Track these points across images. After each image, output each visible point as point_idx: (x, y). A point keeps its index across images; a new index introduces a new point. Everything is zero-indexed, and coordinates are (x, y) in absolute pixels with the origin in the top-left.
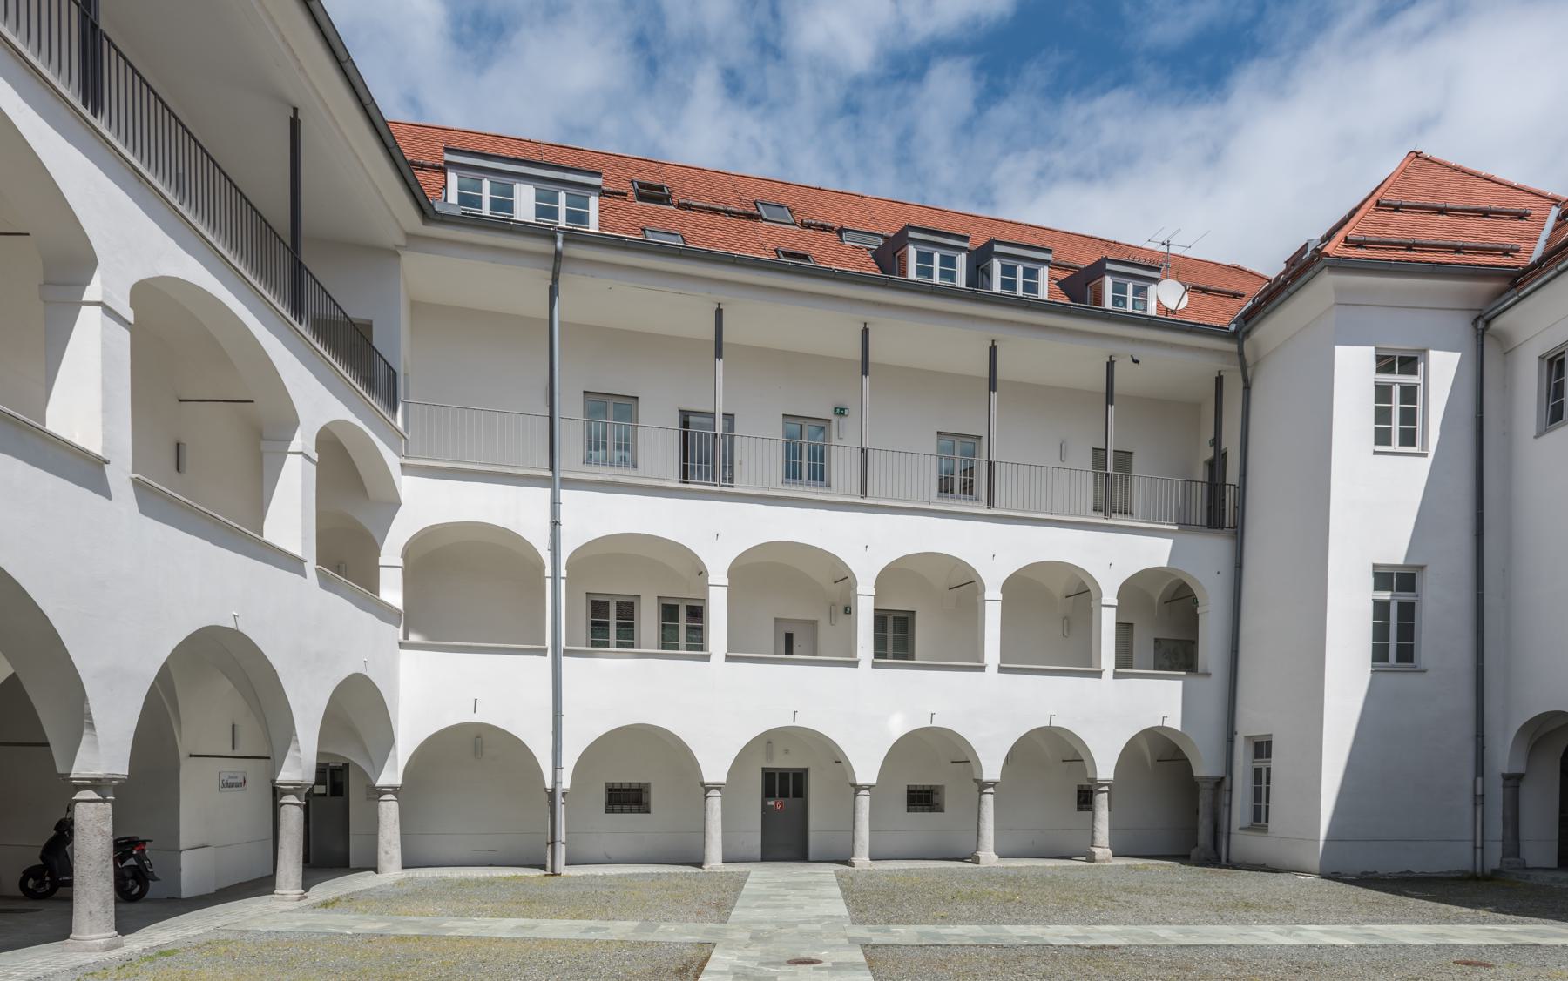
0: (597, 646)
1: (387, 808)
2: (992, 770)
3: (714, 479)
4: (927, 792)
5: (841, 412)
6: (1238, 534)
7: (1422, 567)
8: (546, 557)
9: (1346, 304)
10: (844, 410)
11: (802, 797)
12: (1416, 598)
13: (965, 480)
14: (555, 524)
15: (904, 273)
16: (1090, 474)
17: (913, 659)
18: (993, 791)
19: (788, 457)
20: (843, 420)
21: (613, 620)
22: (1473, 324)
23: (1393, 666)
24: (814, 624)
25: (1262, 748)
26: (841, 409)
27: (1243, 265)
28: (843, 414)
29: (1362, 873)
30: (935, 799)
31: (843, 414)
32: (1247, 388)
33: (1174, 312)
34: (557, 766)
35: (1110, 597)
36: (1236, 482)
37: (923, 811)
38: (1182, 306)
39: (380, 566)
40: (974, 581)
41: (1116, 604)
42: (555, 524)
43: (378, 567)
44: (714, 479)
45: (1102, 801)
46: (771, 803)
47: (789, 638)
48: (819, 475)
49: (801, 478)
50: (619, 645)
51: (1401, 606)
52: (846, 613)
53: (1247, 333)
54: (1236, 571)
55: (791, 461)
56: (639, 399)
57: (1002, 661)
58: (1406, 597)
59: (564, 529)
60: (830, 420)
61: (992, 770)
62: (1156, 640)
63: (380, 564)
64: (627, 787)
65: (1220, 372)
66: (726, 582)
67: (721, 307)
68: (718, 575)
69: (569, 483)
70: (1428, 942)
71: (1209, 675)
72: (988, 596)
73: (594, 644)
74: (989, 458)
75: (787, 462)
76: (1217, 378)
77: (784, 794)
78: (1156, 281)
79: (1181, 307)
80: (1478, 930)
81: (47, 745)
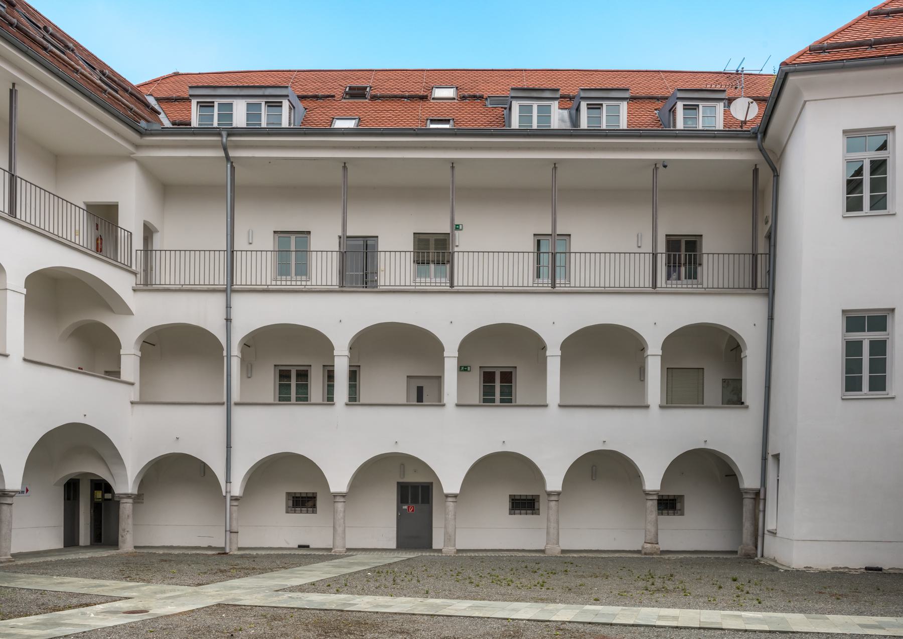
0: (283, 401)
1: (123, 508)
6: (770, 294)
7: (893, 310)
8: (222, 339)
9: (815, 100)
10: (467, 367)
11: (429, 503)
12: (887, 337)
14: (228, 320)
15: (675, 126)
16: (664, 255)
21: (293, 383)
23: (866, 394)
29: (833, 568)
33: (745, 122)
34: (228, 481)
42: (228, 320)
46: (405, 507)
47: (420, 390)
50: (502, 401)
51: (873, 343)
56: (571, 235)
58: (432, 244)
59: (235, 323)
62: (724, 381)
63: (445, 356)
64: (304, 495)
65: (756, 165)
66: (559, 353)
67: (757, 167)
72: (650, 351)
73: (485, 401)
77: (415, 501)
81: (735, 475)
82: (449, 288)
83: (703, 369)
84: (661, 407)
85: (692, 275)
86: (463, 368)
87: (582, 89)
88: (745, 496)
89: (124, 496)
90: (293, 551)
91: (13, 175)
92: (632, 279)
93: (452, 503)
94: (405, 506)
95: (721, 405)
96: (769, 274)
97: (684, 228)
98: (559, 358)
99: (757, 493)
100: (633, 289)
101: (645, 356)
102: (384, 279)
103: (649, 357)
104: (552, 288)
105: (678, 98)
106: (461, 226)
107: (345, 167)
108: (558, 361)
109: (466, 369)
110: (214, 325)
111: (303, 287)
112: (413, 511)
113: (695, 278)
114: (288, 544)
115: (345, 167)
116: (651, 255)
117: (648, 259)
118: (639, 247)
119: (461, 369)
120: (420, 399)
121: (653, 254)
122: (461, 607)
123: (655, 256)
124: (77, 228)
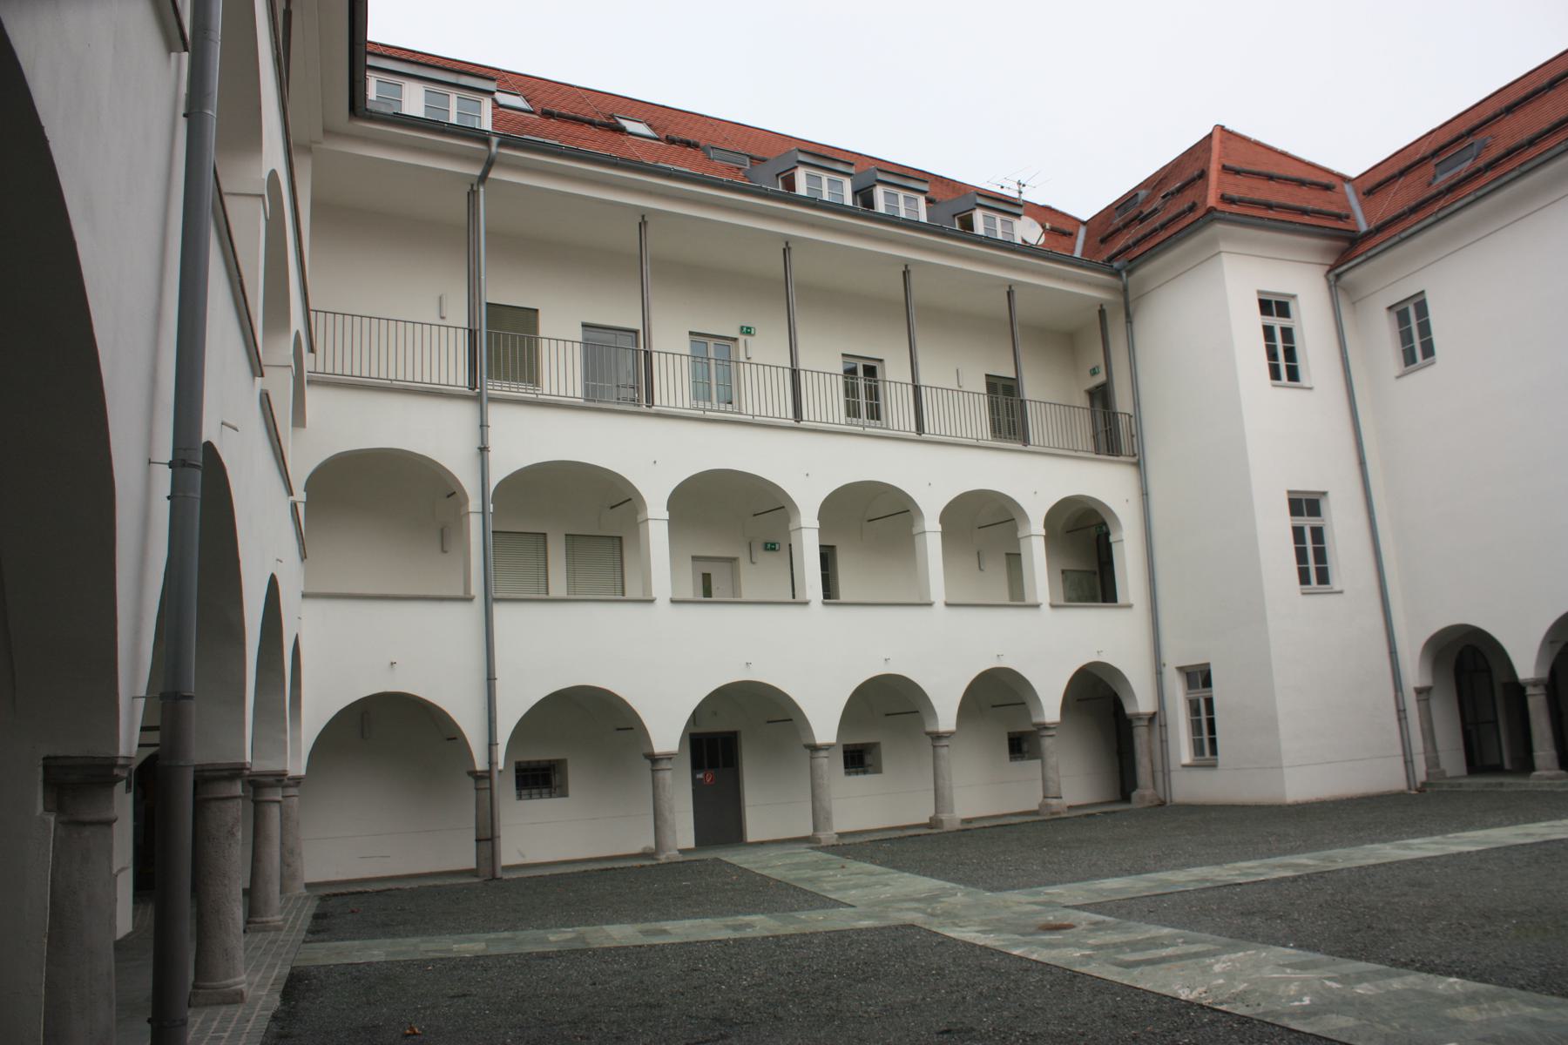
3: (1113, 452)
4: (544, 769)
6: (1139, 465)
7: (1324, 493)
10: (774, 544)
20: (749, 338)
25: (1199, 677)
26: (772, 544)
27: (1054, 206)
31: (750, 332)
36: (1129, 410)
37: (857, 773)
38: (1041, 242)
39: (469, 513)
43: (1018, 540)
44: (1113, 452)
46: (700, 776)
47: (706, 578)
49: (860, 417)
54: (1143, 499)
59: (493, 456)
60: (735, 340)
62: (1063, 572)
65: (1101, 306)
69: (493, 400)
70: (1473, 849)
71: (1130, 606)
75: (877, 399)
77: (713, 765)
78: (1018, 216)
79: (1039, 243)
82: (915, 434)
83: (545, 534)
84: (1053, 606)
86: (769, 546)
88: (1136, 723)
89: (271, 779)
90: (591, 864)
91: (795, 370)
92: (974, 431)
93: (826, 759)
94: (699, 773)
95: (1063, 603)
97: (866, 348)
98: (939, 535)
99: (1152, 718)
100: (453, 388)
101: (462, 513)
102: (662, 400)
104: (470, 389)
106: (753, 330)
107: (643, 224)
108: (938, 537)
110: (455, 457)
111: (389, 382)
112: (711, 781)
113: (878, 418)
114: (523, 856)
115: (643, 224)
116: (467, 331)
117: (462, 338)
118: (748, 358)
120: (707, 592)
121: (470, 331)
123: (472, 334)
124: (1077, 417)
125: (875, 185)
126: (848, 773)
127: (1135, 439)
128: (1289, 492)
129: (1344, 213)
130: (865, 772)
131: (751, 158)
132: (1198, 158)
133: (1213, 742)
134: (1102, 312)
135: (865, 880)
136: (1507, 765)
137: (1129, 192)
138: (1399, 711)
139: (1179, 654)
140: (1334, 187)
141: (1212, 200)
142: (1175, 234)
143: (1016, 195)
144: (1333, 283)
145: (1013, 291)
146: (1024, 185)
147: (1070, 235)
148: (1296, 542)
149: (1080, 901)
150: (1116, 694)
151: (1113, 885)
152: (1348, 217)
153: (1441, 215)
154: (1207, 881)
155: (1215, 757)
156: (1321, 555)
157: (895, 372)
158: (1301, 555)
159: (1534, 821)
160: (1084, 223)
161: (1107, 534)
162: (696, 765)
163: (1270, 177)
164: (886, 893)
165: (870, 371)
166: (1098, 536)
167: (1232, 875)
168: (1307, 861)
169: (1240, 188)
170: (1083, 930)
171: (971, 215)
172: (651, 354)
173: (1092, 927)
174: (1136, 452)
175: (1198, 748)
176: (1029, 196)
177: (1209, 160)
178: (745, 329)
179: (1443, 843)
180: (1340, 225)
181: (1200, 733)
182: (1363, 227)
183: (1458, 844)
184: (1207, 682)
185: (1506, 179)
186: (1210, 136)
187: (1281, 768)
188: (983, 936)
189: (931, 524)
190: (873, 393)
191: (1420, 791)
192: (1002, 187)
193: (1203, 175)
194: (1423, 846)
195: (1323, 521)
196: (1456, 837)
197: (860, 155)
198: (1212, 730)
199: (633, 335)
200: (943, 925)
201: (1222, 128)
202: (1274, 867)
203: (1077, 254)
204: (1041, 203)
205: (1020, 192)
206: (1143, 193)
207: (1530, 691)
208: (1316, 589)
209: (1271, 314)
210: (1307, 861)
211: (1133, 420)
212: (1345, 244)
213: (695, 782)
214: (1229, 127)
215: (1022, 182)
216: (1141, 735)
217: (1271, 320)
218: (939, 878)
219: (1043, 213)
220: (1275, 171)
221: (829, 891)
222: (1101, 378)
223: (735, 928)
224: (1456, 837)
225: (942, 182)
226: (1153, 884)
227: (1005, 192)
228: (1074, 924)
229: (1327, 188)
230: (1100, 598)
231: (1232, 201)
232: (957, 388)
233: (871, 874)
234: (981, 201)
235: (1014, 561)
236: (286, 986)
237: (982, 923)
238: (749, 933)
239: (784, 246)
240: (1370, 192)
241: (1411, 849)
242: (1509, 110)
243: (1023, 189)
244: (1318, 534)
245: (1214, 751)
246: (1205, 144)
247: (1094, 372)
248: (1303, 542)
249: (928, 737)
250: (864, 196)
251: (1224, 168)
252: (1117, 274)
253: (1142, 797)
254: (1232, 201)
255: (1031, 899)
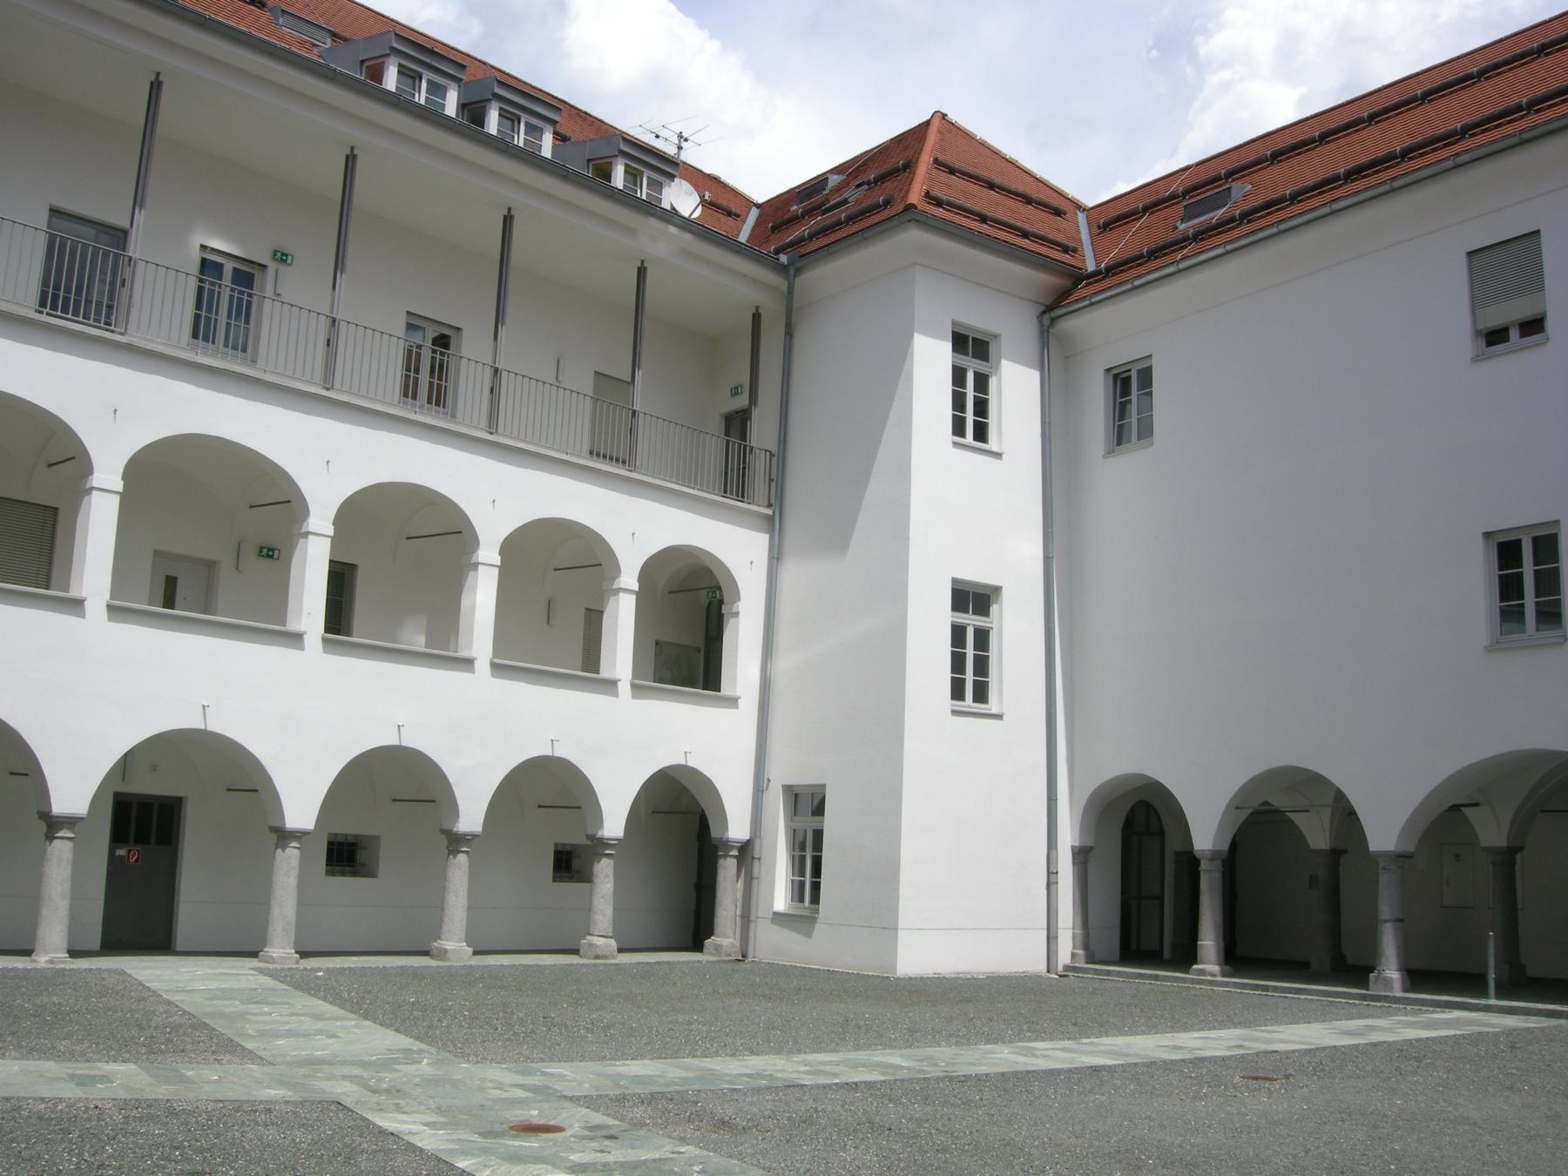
2: (471, 816)
3: (743, 497)
5: (282, 257)
10: (273, 550)
13: (440, 378)
17: (351, 636)
18: (297, 845)
19: (408, 370)
20: (283, 269)
22: (1038, 317)
24: (210, 567)
26: (269, 550)
28: (285, 261)
30: (361, 856)
31: (285, 261)
32: (789, 333)
35: (321, 521)
37: (343, 874)
38: (695, 215)
40: (600, 565)
41: (121, 490)
45: (604, 869)
46: (121, 852)
48: (438, 398)
52: (260, 555)
53: (799, 271)
55: (204, 314)
57: (113, 595)
60: (265, 267)
61: (471, 816)
62: (657, 643)
65: (757, 308)
66: (119, 486)
68: (108, 474)
70: (1110, 1062)
72: (97, 479)
74: (332, 312)
75: (406, 375)
76: (754, 314)
77: (142, 838)
79: (693, 216)
80: (955, 1071)
85: (241, 345)
87: (498, 81)
96: (770, 477)
103: (94, 493)
105: (394, 50)
106: (290, 258)
109: (271, 553)
112: (137, 860)
119: (261, 551)
122: (1491, 951)
125: (489, 100)
126: (329, 873)
127: (773, 485)
128: (955, 581)
129: (1071, 244)
130: (355, 874)
131: (334, 35)
132: (907, 148)
133: (816, 887)
134: (757, 317)
135: (308, 1025)
136: (1167, 954)
137: (818, 176)
138: (1049, 873)
139: (785, 770)
140: (1065, 214)
141: (915, 197)
142: (861, 230)
143: (671, 150)
144: (1046, 328)
145: (645, 268)
146: (686, 140)
147: (737, 216)
148: (954, 670)
149: (587, 1090)
150: (703, 811)
151: (640, 1069)
152: (1075, 251)
153: (1183, 265)
154: (764, 1077)
155: (817, 906)
156: (982, 666)
157: (473, 349)
158: (958, 663)
159: (1185, 1028)
160: (758, 206)
161: (721, 602)
162: (119, 835)
163: (991, 186)
164: (324, 1047)
165: (442, 341)
166: (710, 603)
167: (798, 1072)
168: (898, 1061)
169: (954, 189)
170: (572, 1136)
171: (611, 163)
172: (135, 262)
173: (586, 1133)
174: (773, 501)
175: (798, 892)
176: (690, 156)
177: (919, 152)
178: (279, 255)
179: (1074, 1051)
180: (1066, 258)
181: (802, 874)
182: (1091, 266)
183: (1091, 1053)
184: (819, 810)
185: (1261, 235)
186: (927, 124)
187: (897, 929)
188: (429, 1131)
189: (489, 553)
190: (439, 370)
191: (1060, 976)
192: (657, 137)
193: (909, 167)
194: (1049, 1053)
195: (991, 623)
196: (1092, 1043)
197: (485, 63)
198: (817, 871)
199: (121, 235)
200: (381, 1109)
201: (944, 116)
202: (856, 1066)
203: (743, 238)
204: (707, 170)
205: (680, 148)
206: (835, 180)
207: (1204, 866)
208: (969, 706)
209: (966, 611)
210: (898, 1061)
211: (775, 460)
212: (1065, 282)
213: (112, 859)
214: (952, 117)
215: (685, 135)
216: (727, 868)
217: (965, 361)
218: (407, 1033)
219: (704, 182)
220: (998, 180)
221: (249, 1036)
222: (742, 401)
223: (83, 1081)
224: (1092, 1043)
225: (585, 120)
226: (691, 1074)
227: (659, 145)
228: (563, 1125)
229: (1058, 213)
230: (701, 683)
231: (939, 203)
232: (555, 383)
233: (318, 1017)
234: (624, 147)
235: (593, 621)
236: (510, 966)
237: (439, 1111)
238: (100, 1091)
239: (349, 153)
240: (1106, 227)
241: (1036, 1056)
242: (1276, 157)
243: (684, 145)
244: (982, 637)
245: (815, 899)
246: (919, 133)
247: (735, 392)
248: (963, 671)
249: (443, 836)
250: (473, 112)
251: (936, 161)
252: (782, 270)
253: (718, 948)
254: (939, 203)
255: (520, 1079)
